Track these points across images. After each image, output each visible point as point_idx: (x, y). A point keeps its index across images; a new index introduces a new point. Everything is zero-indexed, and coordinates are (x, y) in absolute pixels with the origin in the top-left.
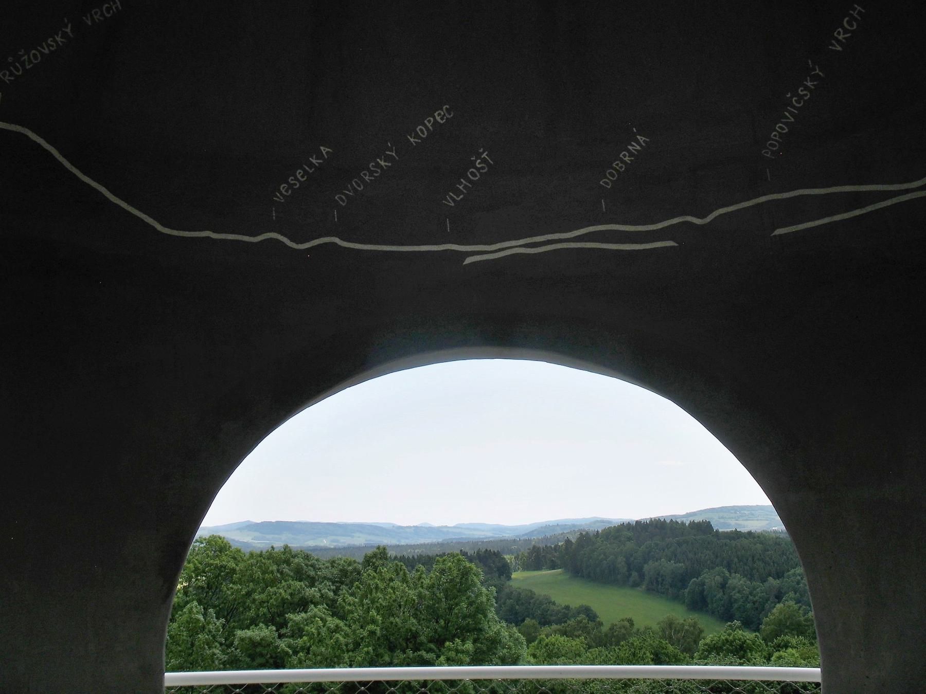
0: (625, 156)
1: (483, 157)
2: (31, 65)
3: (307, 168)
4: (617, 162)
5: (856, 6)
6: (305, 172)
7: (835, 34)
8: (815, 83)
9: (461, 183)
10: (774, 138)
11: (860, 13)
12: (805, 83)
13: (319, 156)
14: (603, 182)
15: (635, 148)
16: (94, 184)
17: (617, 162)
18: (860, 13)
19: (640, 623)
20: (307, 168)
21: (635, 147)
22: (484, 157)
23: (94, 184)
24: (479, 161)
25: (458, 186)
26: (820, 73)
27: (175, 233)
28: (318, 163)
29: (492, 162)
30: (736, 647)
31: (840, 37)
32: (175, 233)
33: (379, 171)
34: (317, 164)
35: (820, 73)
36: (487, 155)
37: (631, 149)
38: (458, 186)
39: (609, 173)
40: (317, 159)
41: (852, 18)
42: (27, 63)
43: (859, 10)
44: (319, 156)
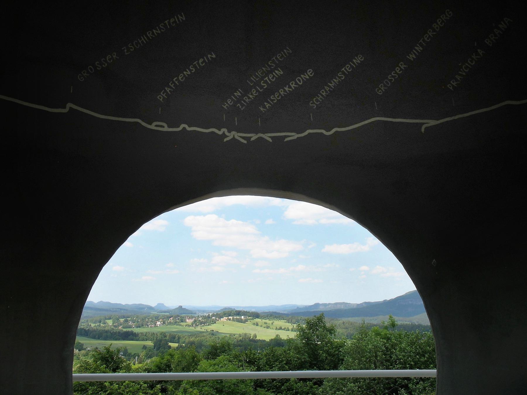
0: (281, 91)
2: (244, 107)
3: (259, 89)
4: (84, 71)
6: (257, 91)
9: (225, 105)
10: (322, 93)
12: (260, 108)
13: (264, 107)
14: (239, 105)
15: (418, 48)
16: (493, 107)
17: (84, 71)
20: (259, 89)
23: (493, 107)
24: (262, 81)
25: (223, 106)
29: (258, 87)
33: (93, 71)
37: (417, 49)
38: (223, 106)
44: (264, 107)
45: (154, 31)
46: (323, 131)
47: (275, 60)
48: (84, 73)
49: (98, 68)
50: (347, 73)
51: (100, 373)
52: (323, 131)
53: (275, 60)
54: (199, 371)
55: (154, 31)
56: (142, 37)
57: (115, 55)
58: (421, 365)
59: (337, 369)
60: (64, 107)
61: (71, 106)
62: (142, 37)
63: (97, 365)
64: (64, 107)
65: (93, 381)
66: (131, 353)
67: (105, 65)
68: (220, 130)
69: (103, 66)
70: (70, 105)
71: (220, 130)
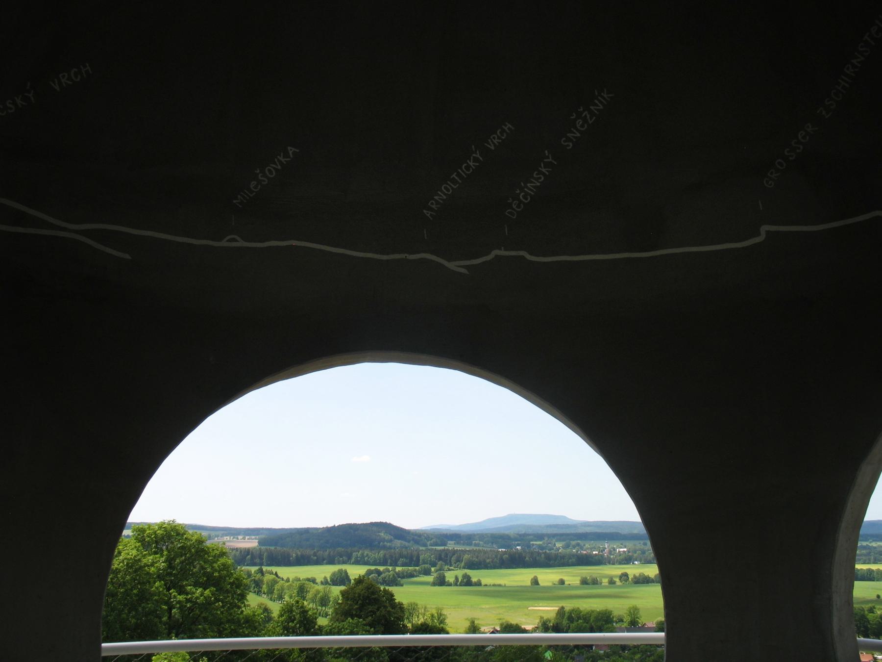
1: (452, 177)
5: (87, 65)
7: (61, 75)
8: (24, 104)
11: (509, 129)
13: (286, 155)
18: (509, 129)
19: (400, 570)
21: (534, 183)
22: (454, 178)
26: (32, 99)
27: (385, 257)
28: (285, 161)
30: (233, 603)
31: (63, 80)
32: (385, 257)
33: (785, 165)
34: (285, 163)
35: (32, 99)
36: (456, 175)
39: (445, 188)
40: (284, 157)
41: (503, 131)
42: (588, 116)
43: (509, 127)
45: (854, 61)
46: (529, 257)
47: (456, 178)
48: (772, 173)
49: (791, 158)
50: (465, 176)
51: (281, 636)
52: (529, 257)
53: (456, 178)
54: (480, 633)
55: (854, 61)
56: (840, 81)
57: (810, 126)
58: (274, 621)
59: (475, 633)
60: (759, 234)
61: (767, 229)
62: (840, 81)
63: (221, 623)
64: (759, 234)
65: (373, 646)
66: (611, 611)
67: (799, 148)
68: (768, 232)
69: (798, 151)
70: (764, 228)
71: (768, 232)
